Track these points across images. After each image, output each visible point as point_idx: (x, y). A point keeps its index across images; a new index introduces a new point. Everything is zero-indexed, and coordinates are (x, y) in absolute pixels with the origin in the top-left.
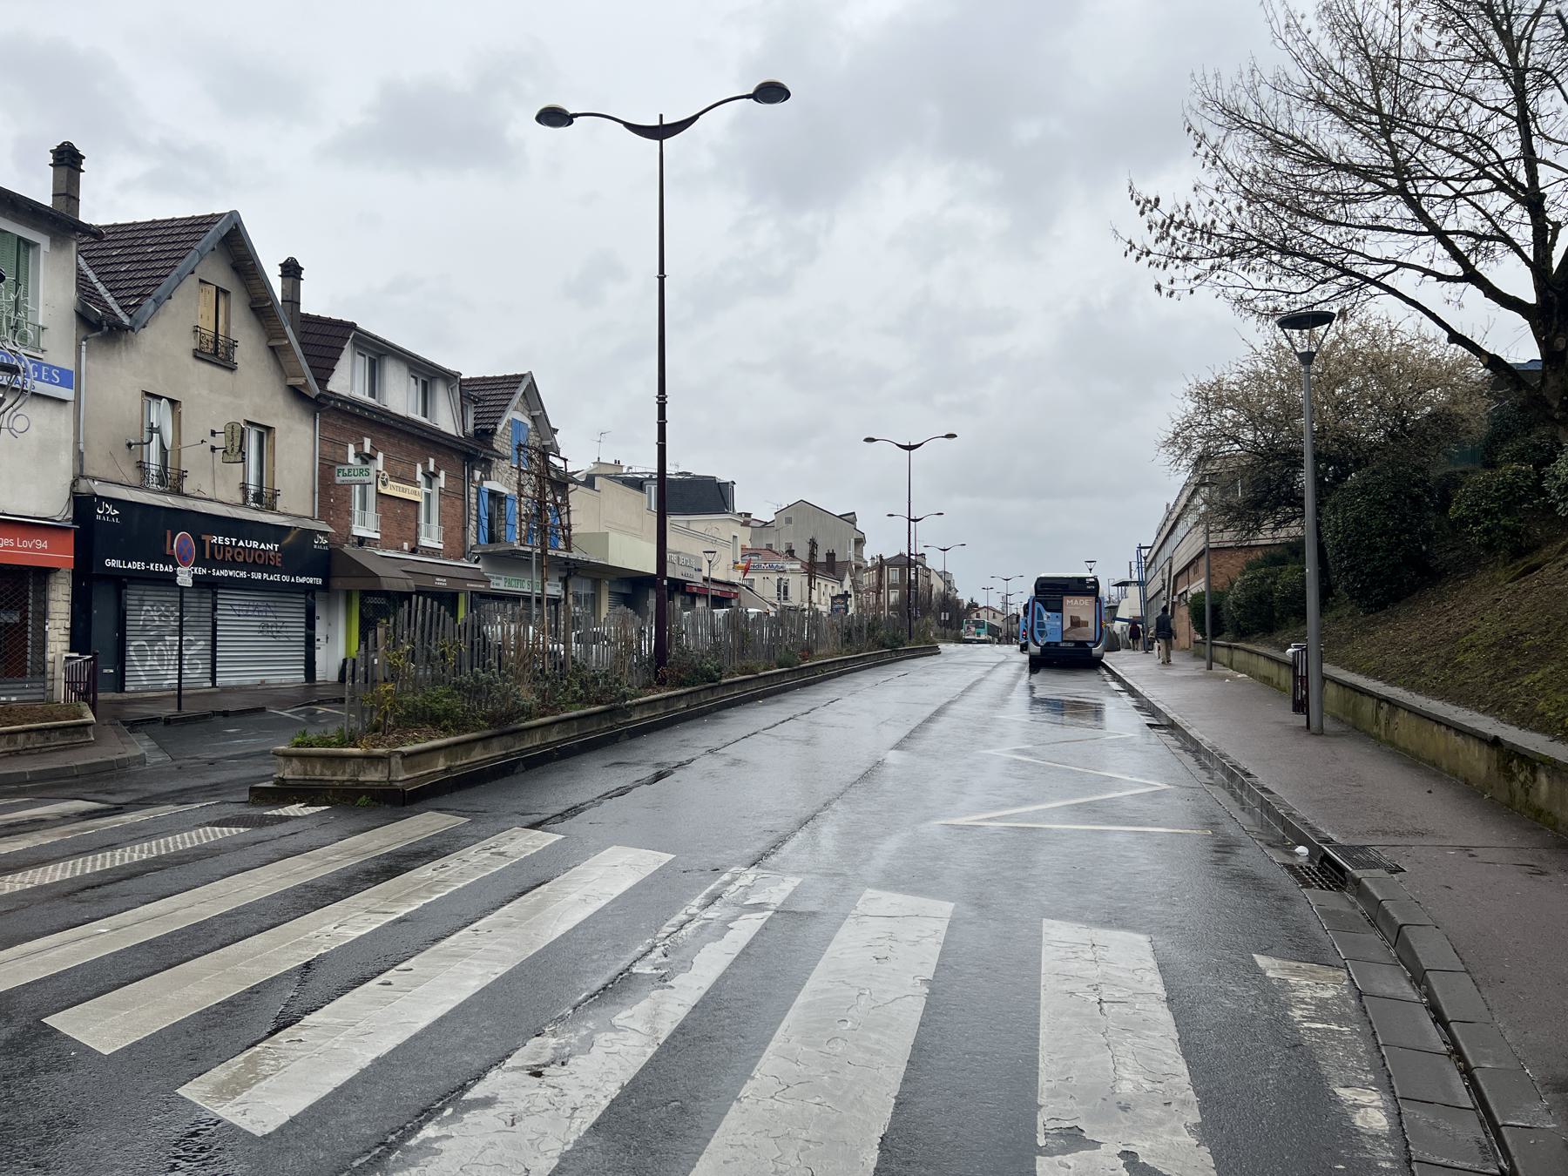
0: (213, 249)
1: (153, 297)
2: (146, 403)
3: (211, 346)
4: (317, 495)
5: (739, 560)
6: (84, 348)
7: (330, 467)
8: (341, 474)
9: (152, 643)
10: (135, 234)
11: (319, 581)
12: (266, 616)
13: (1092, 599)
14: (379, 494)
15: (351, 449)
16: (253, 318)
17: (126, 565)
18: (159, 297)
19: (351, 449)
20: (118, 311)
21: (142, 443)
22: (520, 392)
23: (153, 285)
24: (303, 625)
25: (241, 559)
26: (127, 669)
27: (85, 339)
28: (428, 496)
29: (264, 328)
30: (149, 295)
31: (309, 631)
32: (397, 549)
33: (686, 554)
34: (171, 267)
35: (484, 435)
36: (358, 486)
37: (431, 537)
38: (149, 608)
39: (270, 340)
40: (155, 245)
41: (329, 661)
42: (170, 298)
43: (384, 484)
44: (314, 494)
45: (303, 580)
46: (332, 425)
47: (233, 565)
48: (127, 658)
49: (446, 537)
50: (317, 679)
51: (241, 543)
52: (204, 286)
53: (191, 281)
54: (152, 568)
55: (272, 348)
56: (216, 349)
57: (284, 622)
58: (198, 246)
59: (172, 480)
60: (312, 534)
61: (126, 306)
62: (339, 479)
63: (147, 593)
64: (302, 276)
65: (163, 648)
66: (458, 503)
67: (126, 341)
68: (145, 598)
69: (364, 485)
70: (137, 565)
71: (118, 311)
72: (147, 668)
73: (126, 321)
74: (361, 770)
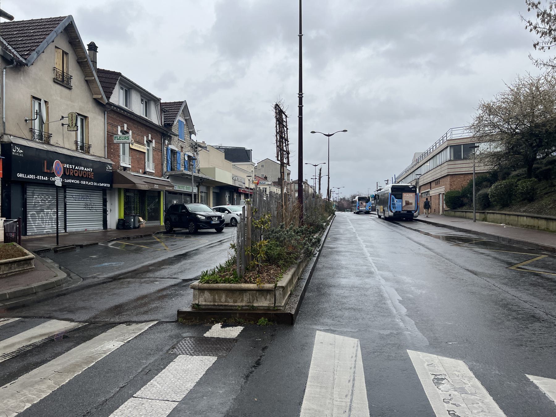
0: (62, 32)
1: (36, 51)
2: (33, 101)
3: (61, 77)
4: (106, 148)
5: (254, 180)
6: (4, 73)
7: (111, 136)
8: (116, 139)
9: (38, 213)
10: (24, 25)
11: (109, 185)
12: (87, 201)
13: (414, 194)
14: (130, 149)
15: (119, 129)
16: (78, 67)
17: (27, 176)
18: (39, 51)
19: (119, 129)
20: (21, 59)
21: (32, 120)
22: (182, 108)
23: (35, 46)
24: (102, 204)
25: (77, 175)
26: (28, 225)
27: (5, 68)
28: (148, 150)
29: (83, 72)
30: (34, 50)
31: (104, 207)
32: (138, 172)
33: (241, 177)
34: (43, 38)
35: (168, 126)
36: (121, 144)
37: (150, 168)
38: (37, 197)
39: (86, 77)
40: (34, 29)
41: (113, 219)
42: (43, 52)
43: (132, 144)
44: (105, 147)
45: (102, 185)
46: (111, 117)
47: (74, 177)
48: (27, 220)
49: (156, 168)
50: (108, 228)
51: (77, 168)
52: (57, 50)
53: (52, 46)
54: (38, 178)
55: (87, 81)
56: (63, 79)
57: (94, 203)
58: (55, 30)
59: (45, 138)
60: (105, 164)
61: (23, 55)
62: (115, 141)
63: (36, 190)
64: (97, 51)
65: (43, 215)
66: (160, 154)
67: (23, 72)
68: (35, 192)
69: (124, 144)
70: (31, 177)
71: (19, 57)
72: (36, 224)
73: (24, 61)
74: (255, 298)
